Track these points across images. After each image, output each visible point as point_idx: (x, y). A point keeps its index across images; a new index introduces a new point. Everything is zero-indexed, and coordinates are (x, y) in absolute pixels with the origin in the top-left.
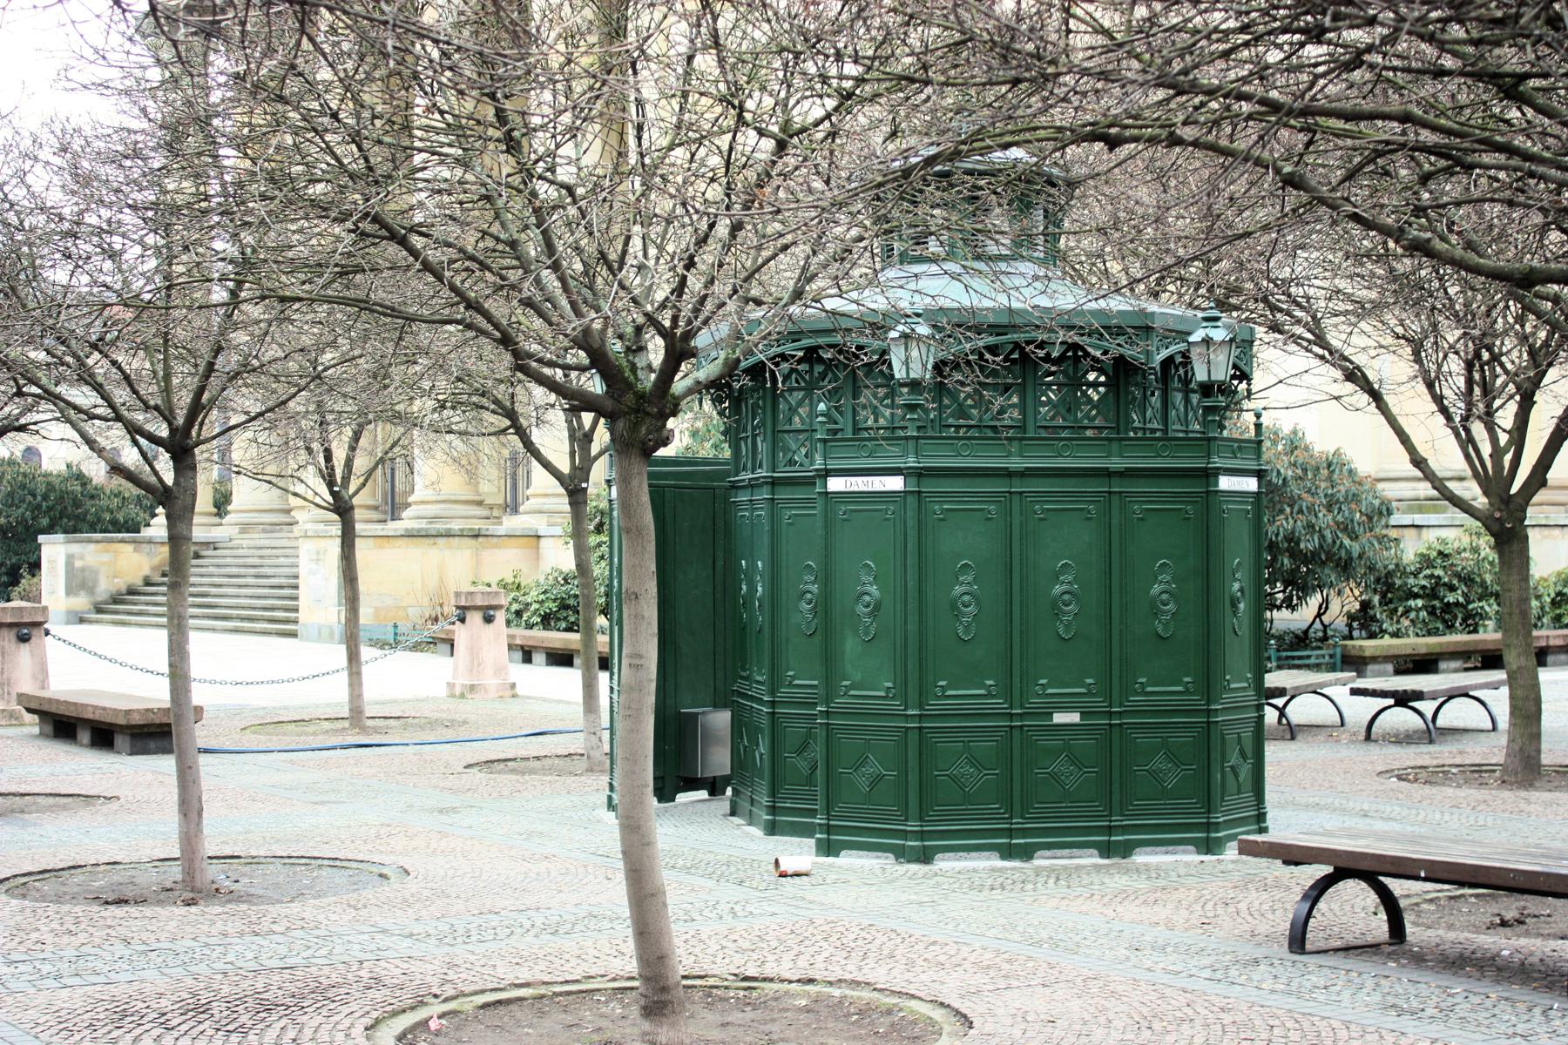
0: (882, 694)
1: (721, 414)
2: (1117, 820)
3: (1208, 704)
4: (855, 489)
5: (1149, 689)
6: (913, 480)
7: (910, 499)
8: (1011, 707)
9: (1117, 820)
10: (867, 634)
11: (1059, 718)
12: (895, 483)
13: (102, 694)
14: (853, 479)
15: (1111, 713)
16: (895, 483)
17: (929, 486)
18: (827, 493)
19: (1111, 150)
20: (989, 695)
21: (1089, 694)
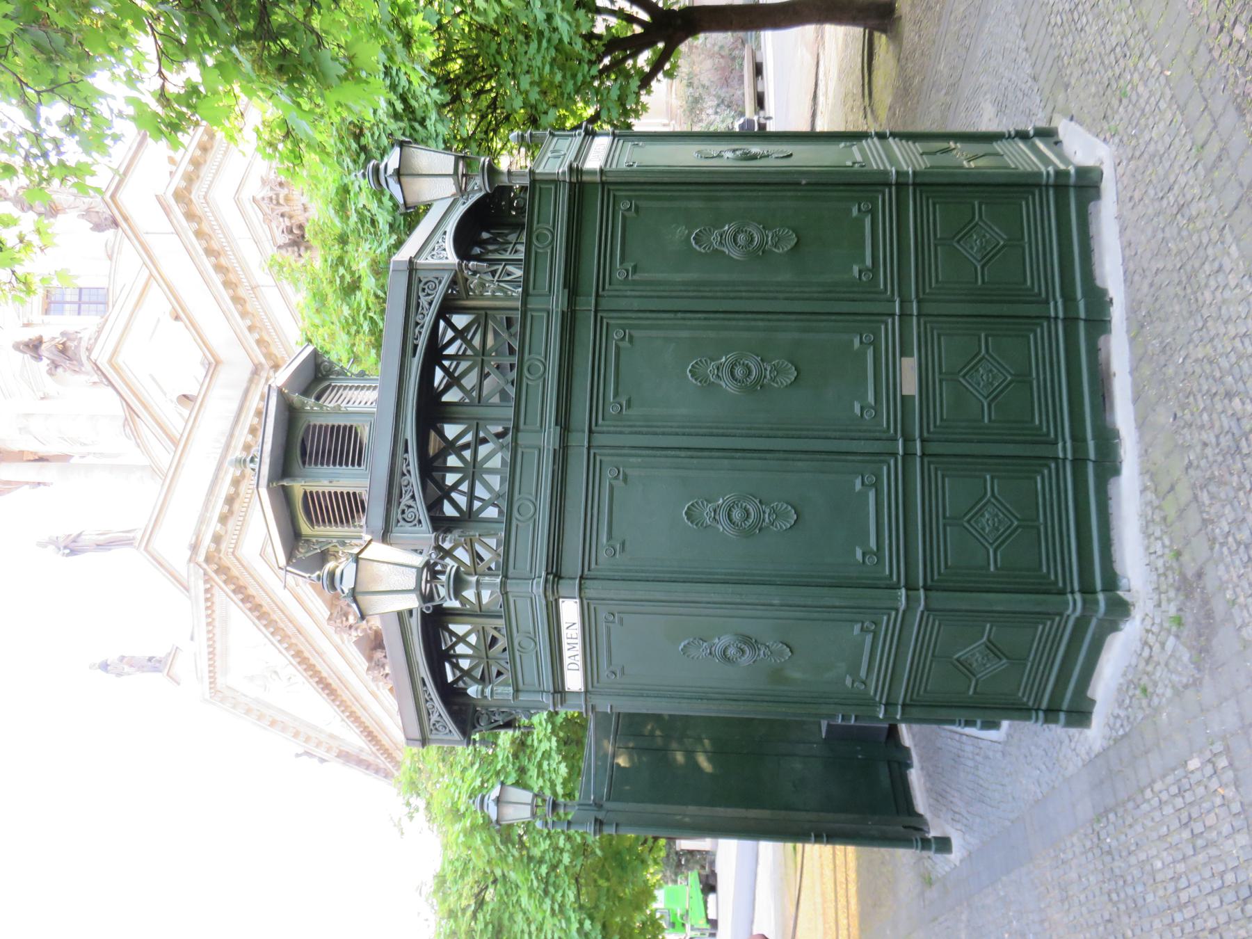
0: (869, 638)
1: (560, 911)
2: (1064, 449)
3: (889, 185)
4: (579, 659)
5: (869, 262)
6: (564, 586)
7: (590, 593)
8: (895, 455)
9: (1064, 449)
10: (781, 654)
11: (910, 386)
12: (570, 610)
13: (1132, 417)
14: (566, 661)
15: (905, 454)
16: (570, 610)
17: (572, 563)
18: (586, 692)
19: (383, 648)
20: (877, 486)
21: (873, 212)
